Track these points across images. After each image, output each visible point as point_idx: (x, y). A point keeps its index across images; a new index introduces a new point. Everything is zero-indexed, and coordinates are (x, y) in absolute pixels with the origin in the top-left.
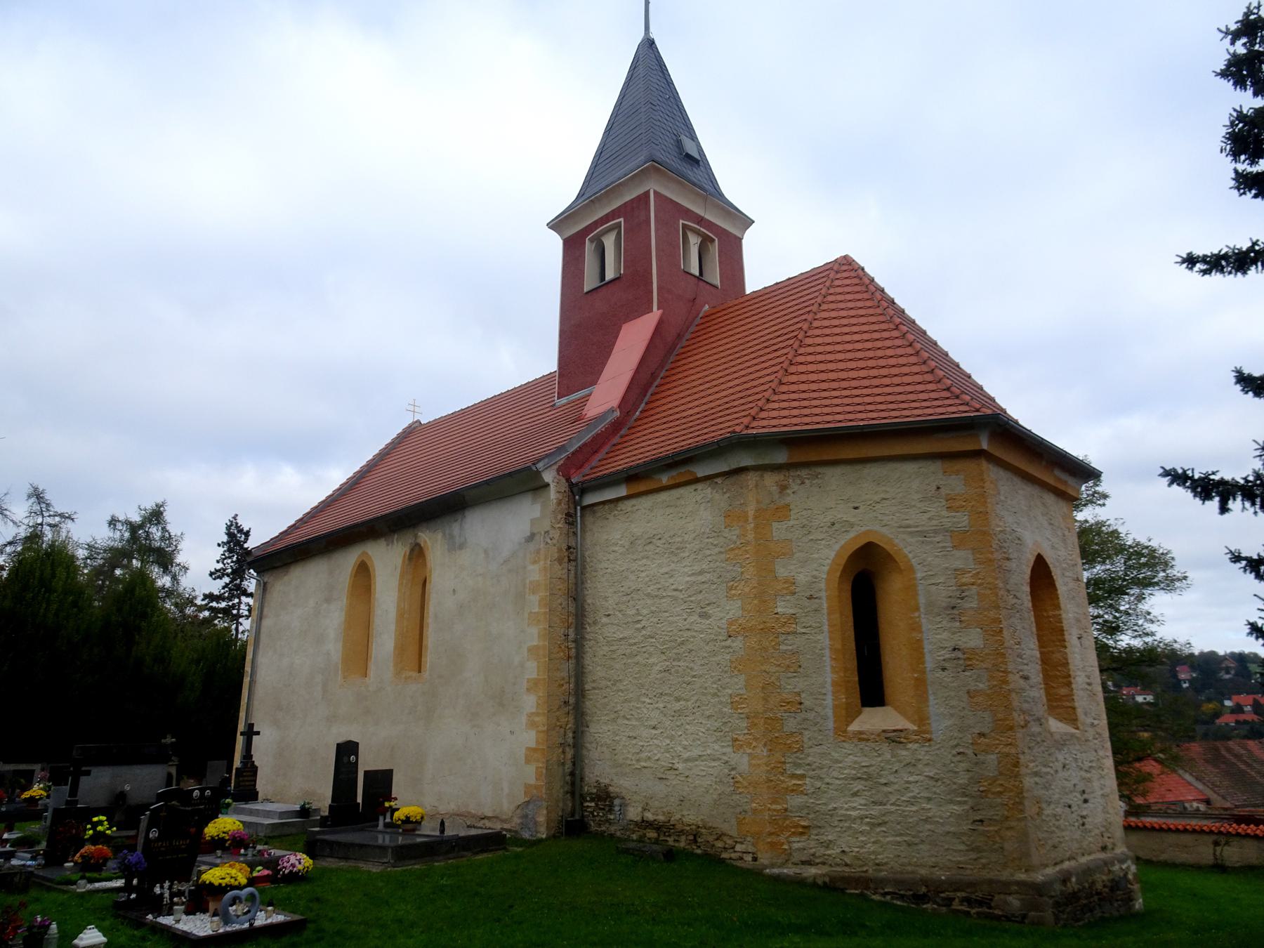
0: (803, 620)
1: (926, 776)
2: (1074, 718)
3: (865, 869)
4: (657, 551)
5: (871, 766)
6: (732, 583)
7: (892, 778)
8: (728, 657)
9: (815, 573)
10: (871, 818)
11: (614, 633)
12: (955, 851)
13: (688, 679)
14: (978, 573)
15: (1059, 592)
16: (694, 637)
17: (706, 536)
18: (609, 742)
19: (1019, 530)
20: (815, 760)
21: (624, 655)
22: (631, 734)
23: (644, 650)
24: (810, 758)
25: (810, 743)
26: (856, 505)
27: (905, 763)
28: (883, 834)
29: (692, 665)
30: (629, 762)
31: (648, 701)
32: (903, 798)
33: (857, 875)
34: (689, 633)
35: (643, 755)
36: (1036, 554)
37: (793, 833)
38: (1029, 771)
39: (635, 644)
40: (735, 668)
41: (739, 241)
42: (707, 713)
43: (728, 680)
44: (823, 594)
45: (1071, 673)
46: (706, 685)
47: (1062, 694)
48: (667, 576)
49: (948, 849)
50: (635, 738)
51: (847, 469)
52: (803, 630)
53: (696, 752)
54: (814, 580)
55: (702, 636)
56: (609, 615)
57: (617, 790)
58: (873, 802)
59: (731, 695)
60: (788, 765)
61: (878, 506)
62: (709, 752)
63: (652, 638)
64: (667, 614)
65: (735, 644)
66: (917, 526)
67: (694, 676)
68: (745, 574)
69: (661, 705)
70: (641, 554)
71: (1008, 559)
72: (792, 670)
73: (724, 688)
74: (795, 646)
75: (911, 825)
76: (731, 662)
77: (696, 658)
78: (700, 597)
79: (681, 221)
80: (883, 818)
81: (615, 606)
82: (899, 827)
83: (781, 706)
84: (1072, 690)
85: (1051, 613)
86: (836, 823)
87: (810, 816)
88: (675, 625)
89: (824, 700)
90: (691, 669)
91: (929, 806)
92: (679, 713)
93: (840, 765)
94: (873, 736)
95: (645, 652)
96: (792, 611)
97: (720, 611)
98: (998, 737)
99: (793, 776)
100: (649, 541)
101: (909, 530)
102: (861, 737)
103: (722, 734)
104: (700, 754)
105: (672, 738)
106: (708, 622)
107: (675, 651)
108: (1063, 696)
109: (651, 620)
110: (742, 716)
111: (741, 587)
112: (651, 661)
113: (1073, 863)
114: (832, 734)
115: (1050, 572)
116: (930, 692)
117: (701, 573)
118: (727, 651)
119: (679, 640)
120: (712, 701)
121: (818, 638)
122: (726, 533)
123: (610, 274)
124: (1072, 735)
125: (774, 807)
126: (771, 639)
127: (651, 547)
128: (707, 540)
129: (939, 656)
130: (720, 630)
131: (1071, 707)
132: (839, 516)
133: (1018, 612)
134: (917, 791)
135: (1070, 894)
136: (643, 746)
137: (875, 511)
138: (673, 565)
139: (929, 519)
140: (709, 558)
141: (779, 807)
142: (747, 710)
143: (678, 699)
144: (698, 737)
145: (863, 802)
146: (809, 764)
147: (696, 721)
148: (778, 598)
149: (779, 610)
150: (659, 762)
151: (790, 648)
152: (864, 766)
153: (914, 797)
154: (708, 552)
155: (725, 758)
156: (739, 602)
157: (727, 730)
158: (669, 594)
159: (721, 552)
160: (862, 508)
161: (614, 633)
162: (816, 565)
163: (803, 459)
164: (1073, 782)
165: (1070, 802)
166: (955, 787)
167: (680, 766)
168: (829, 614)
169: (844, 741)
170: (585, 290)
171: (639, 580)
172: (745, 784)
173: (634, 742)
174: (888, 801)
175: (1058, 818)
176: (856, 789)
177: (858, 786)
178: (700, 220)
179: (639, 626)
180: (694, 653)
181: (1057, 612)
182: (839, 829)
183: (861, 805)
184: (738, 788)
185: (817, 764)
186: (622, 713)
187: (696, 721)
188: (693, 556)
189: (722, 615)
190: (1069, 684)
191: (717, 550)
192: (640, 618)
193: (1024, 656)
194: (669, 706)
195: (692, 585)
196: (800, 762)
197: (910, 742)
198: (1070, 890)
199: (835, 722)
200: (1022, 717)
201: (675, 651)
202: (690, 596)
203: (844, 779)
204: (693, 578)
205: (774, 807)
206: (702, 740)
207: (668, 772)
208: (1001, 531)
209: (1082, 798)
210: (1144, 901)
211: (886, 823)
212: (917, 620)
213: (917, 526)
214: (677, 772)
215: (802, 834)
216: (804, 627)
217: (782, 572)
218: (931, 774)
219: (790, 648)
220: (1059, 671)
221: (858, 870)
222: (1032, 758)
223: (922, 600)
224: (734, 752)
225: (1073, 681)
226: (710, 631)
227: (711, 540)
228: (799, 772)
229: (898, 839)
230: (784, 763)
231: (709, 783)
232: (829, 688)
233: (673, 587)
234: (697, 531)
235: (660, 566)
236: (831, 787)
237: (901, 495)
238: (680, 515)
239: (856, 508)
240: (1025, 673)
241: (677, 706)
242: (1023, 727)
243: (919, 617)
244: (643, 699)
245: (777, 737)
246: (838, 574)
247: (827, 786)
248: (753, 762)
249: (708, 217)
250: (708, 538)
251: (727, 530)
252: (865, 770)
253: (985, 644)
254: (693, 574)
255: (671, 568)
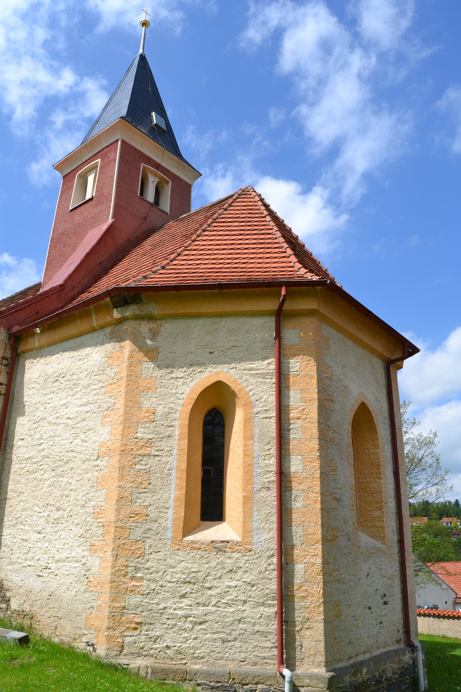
0: (158, 444)
1: (244, 582)
2: (382, 535)
3: (184, 662)
4: (60, 387)
5: (198, 572)
6: (107, 412)
7: (215, 583)
8: (96, 474)
9: (171, 405)
10: (194, 617)
11: (24, 453)
12: (263, 648)
13: (66, 492)
14: (304, 409)
15: (379, 435)
16: (76, 457)
17: (94, 374)
18: (9, 544)
19: (346, 380)
20: (152, 565)
21: (28, 471)
22: (25, 537)
23: (41, 467)
24: (149, 563)
25: (151, 551)
26: (212, 350)
27: (228, 569)
28: (202, 631)
29: (71, 480)
30: (20, 561)
31: (38, 510)
32: (223, 601)
33: (176, 667)
34: (73, 454)
35: (30, 555)
36: (360, 402)
37: (128, 628)
38: (332, 579)
39: (36, 463)
40: (100, 483)
41: (188, 187)
42: (76, 521)
43: (94, 493)
44: (177, 423)
45: (383, 499)
46: (78, 498)
47: (375, 516)
48: (64, 407)
49: (256, 646)
50: (26, 541)
51: (208, 321)
52: (156, 453)
53: (65, 555)
54: (170, 411)
55: (80, 456)
56: (22, 440)
57: (9, 584)
58: (197, 603)
59: (94, 506)
60: (130, 569)
61: (229, 352)
62: (73, 554)
63: (48, 458)
64: (60, 438)
65: (102, 463)
66: (259, 369)
67: (71, 490)
68: (117, 405)
69: (46, 514)
70: (50, 390)
71: (332, 401)
72: (143, 486)
73: (90, 501)
74: (148, 466)
75: (227, 624)
76: (98, 478)
77: (75, 475)
78: (84, 423)
79: (142, 164)
80: (204, 618)
81: (27, 432)
82: (216, 625)
83: (131, 517)
84: (383, 513)
85: (371, 451)
86: (165, 621)
87: (144, 614)
88: (64, 447)
89: (167, 513)
90: (70, 484)
91: (244, 608)
92: (57, 521)
93: (174, 570)
94: (203, 546)
95: (42, 470)
96: (150, 436)
97: (96, 436)
98: (307, 549)
99: (133, 578)
100: (56, 379)
101: (252, 372)
102: (194, 546)
103: (85, 539)
104: (67, 556)
105: (50, 541)
106: (86, 445)
107: (61, 469)
108: (377, 518)
109: (49, 443)
110: (100, 524)
111: (112, 415)
112: (45, 476)
113: (367, 656)
114: (169, 543)
115: (372, 418)
116: (255, 509)
117: (86, 404)
118: (96, 469)
119: (65, 459)
120: (81, 511)
121: (168, 459)
122: (108, 371)
123: (88, 196)
124: (379, 549)
125: (114, 604)
126: (129, 459)
127: (57, 384)
128: (95, 377)
129: (266, 478)
130: (93, 452)
131: (380, 527)
132: (197, 359)
133: (336, 445)
134: (235, 595)
135: (359, 683)
136: (30, 548)
137: (226, 356)
138: (70, 398)
139: (268, 364)
140: (94, 392)
141: (118, 605)
142: (104, 520)
143: (58, 509)
144: (68, 541)
145: (189, 603)
146: (147, 569)
147: (68, 528)
148: (140, 425)
149: (139, 435)
150: (39, 562)
151: (144, 467)
152: (192, 572)
153: (233, 600)
154: (94, 387)
155: (84, 560)
156: (109, 428)
157: (88, 536)
158: (64, 422)
159: (102, 387)
160: (215, 354)
161: (24, 453)
162: (173, 399)
163: (172, 311)
164: (375, 588)
165: (370, 604)
166: (267, 591)
167: (53, 566)
168: (180, 440)
169: (179, 549)
170: (70, 209)
171: (46, 410)
172: (95, 583)
173: (25, 544)
174: (210, 602)
175: (356, 618)
176: (184, 592)
177: (187, 589)
178: (158, 166)
179: (41, 448)
180: (73, 470)
181: (377, 451)
182: (166, 626)
183: (187, 605)
184: (90, 586)
185: (154, 569)
186: (20, 520)
187: (68, 528)
188: (83, 391)
189: (96, 438)
190: (381, 508)
191: (100, 385)
192: (42, 441)
193: (339, 482)
194: (51, 515)
195: (79, 414)
196: (141, 566)
197: (234, 552)
198: (360, 680)
199: (173, 532)
200: (330, 532)
201: (61, 469)
202: (77, 423)
203: (177, 582)
204: (81, 409)
205: (114, 604)
206: (70, 544)
207: (44, 571)
208: (327, 378)
209: (383, 601)
210: (428, 682)
211: (205, 622)
212: (251, 447)
213: (259, 369)
214: (50, 571)
215: (135, 629)
216: (158, 450)
217: (146, 404)
218: (248, 580)
219: (144, 467)
220: (374, 497)
221: (179, 662)
222: (336, 567)
223: (257, 431)
224: (91, 556)
225: (384, 505)
226: (87, 452)
227: (97, 377)
228: (139, 575)
229: (215, 636)
230: (127, 566)
231: (70, 581)
232: (171, 502)
233: (67, 416)
234: (89, 371)
235: (60, 399)
236: (163, 589)
237: (248, 344)
238: (80, 357)
239: (211, 353)
240: (338, 496)
241: (58, 514)
242: (330, 541)
243: (253, 444)
244: (35, 509)
245: (124, 544)
246: (190, 407)
247: (160, 588)
248: (103, 565)
249: (164, 164)
250: (95, 375)
251: (109, 369)
252: (193, 575)
253: (303, 470)
254: (81, 405)
255: (67, 400)
